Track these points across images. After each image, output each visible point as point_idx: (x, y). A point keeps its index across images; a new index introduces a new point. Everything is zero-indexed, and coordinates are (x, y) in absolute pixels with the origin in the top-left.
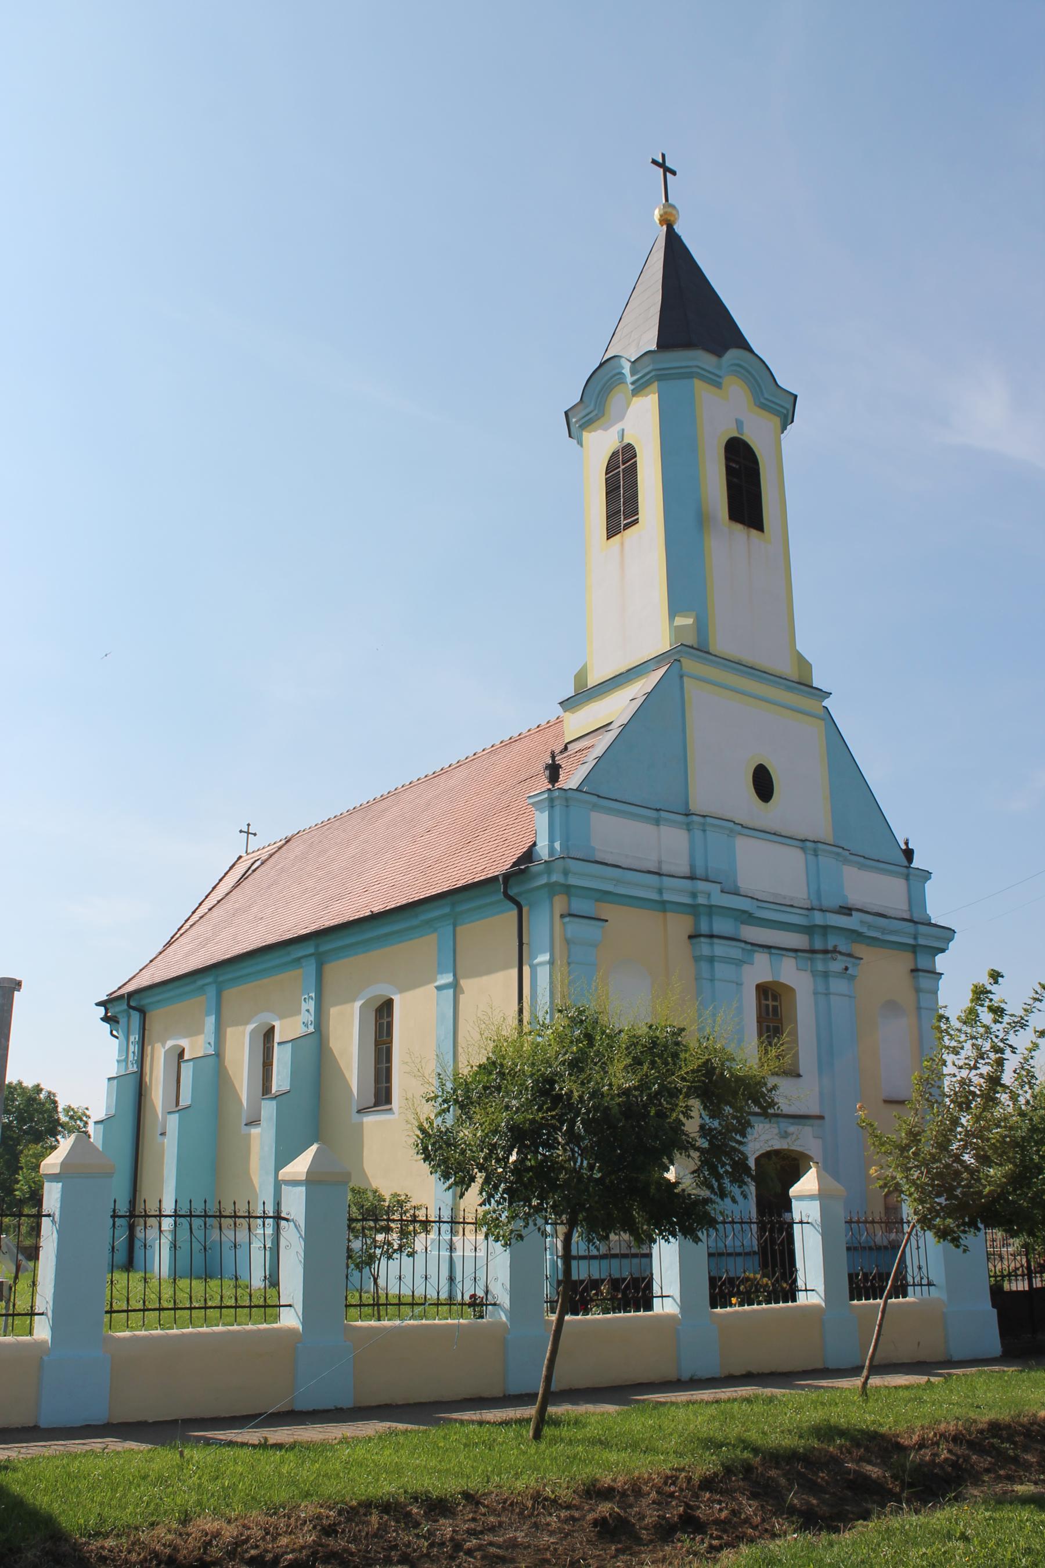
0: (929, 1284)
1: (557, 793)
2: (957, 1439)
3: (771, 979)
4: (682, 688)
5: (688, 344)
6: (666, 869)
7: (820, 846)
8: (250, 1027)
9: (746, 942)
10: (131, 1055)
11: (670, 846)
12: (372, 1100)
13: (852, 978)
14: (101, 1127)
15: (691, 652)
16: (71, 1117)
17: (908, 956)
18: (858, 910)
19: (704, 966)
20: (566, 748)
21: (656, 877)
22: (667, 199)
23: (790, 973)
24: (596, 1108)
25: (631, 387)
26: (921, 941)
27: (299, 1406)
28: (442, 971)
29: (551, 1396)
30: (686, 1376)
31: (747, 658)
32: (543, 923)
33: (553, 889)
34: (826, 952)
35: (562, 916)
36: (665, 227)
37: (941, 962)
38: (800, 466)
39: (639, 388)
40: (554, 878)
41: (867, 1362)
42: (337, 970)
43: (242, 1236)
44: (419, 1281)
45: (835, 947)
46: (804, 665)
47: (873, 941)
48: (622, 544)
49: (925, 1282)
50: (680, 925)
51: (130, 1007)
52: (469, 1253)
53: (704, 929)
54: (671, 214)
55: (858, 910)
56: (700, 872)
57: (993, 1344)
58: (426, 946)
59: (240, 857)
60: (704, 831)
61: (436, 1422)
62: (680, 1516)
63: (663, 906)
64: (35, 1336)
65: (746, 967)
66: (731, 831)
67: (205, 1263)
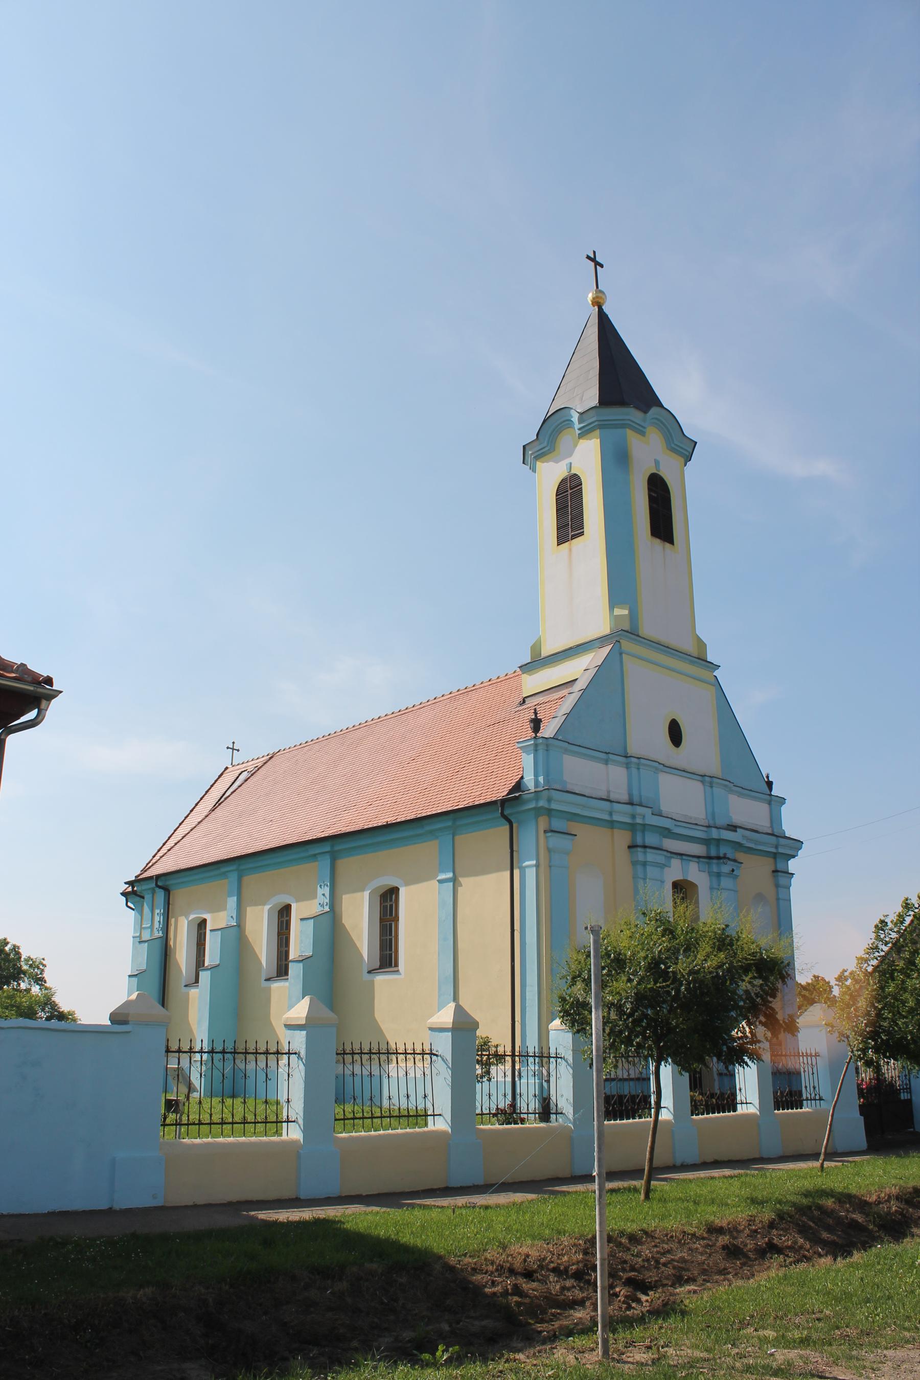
0: (821, 1099)
1: (540, 741)
2: (898, 1198)
3: (681, 878)
4: (621, 662)
5: (622, 403)
6: (613, 797)
7: (715, 780)
8: (267, 907)
9: (667, 851)
10: (156, 925)
11: (613, 779)
12: (378, 965)
13: (737, 876)
14: (135, 980)
15: (625, 635)
16: (31, 966)
17: (771, 860)
18: (740, 827)
19: (640, 868)
20: (524, 701)
21: (608, 803)
22: (597, 287)
23: (696, 874)
24: (694, 981)
25: (578, 432)
26: (781, 850)
27: (765, 1156)
28: (443, 871)
29: (655, 1171)
30: (678, 1163)
31: (663, 639)
32: (530, 837)
33: (538, 812)
34: (718, 858)
35: (545, 832)
36: (596, 308)
37: (792, 865)
38: (698, 494)
39: (585, 433)
40: (542, 803)
41: (823, 1150)
42: (349, 865)
43: (251, 1066)
44: (420, 1100)
45: (725, 854)
46: (701, 645)
47: (750, 850)
48: (570, 550)
49: (817, 1097)
50: (622, 838)
51: (157, 886)
52: (501, 1079)
53: (639, 841)
54: (601, 298)
55: (740, 827)
56: (636, 800)
57: (863, 1144)
58: (427, 850)
59: (227, 768)
60: (638, 769)
61: (400, 1206)
62: (766, 1244)
63: (611, 824)
64: (284, 1137)
65: (666, 869)
66: (657, 769)
67: (231, 1087)
